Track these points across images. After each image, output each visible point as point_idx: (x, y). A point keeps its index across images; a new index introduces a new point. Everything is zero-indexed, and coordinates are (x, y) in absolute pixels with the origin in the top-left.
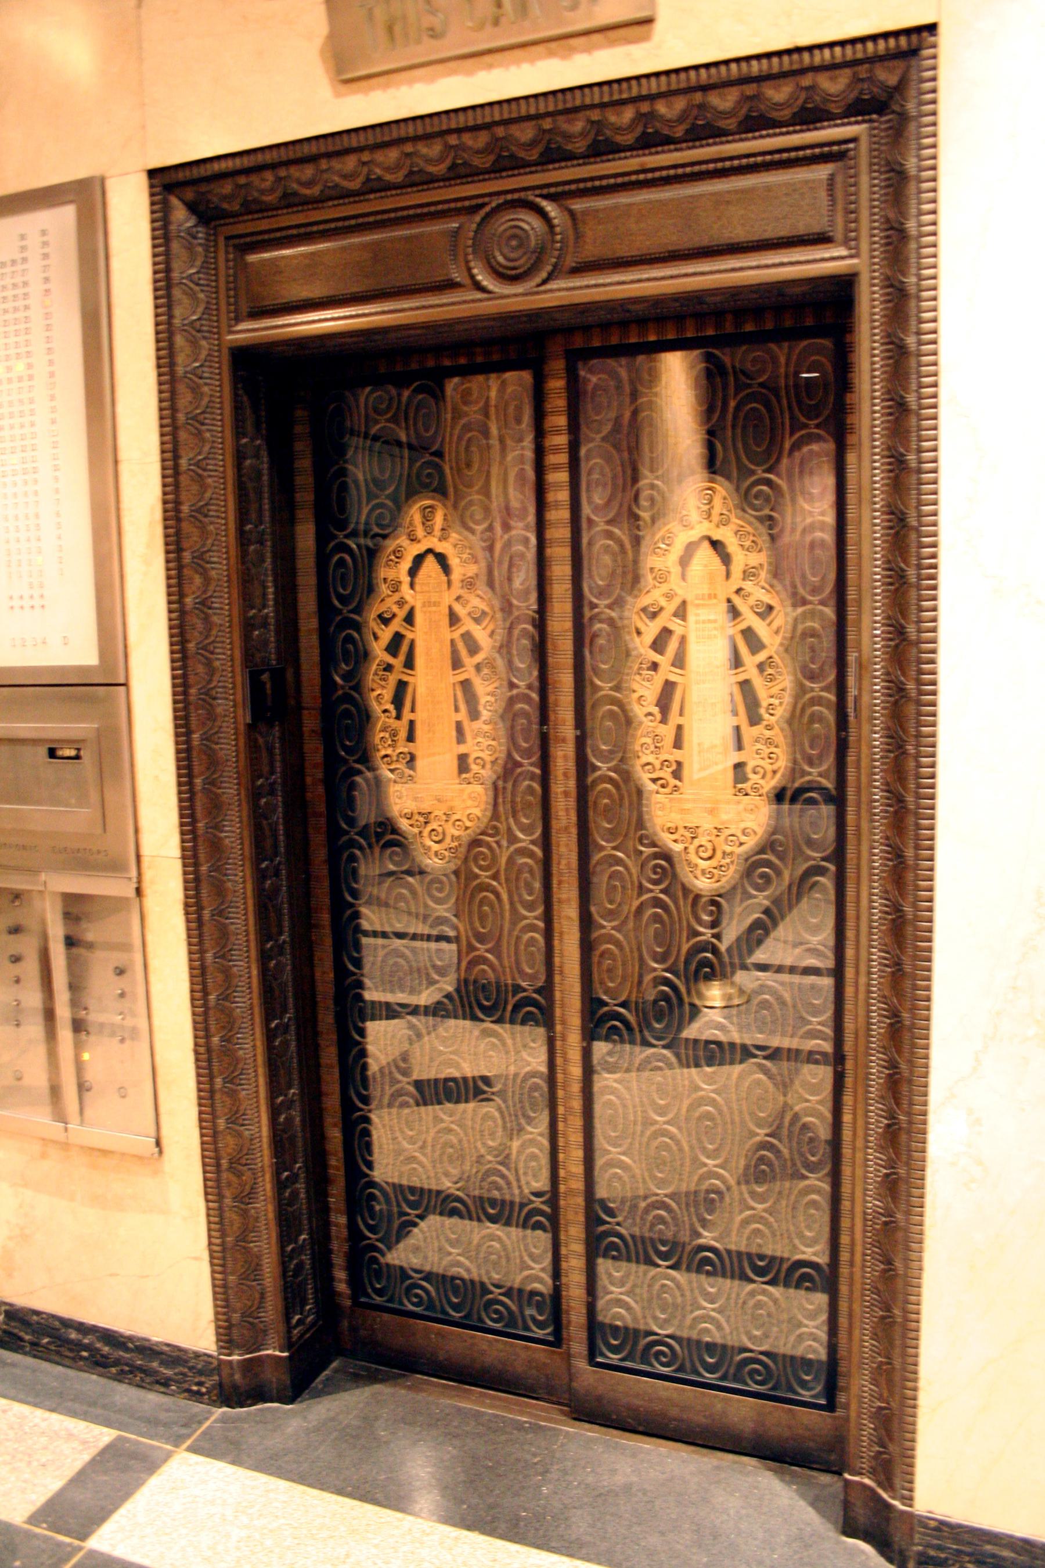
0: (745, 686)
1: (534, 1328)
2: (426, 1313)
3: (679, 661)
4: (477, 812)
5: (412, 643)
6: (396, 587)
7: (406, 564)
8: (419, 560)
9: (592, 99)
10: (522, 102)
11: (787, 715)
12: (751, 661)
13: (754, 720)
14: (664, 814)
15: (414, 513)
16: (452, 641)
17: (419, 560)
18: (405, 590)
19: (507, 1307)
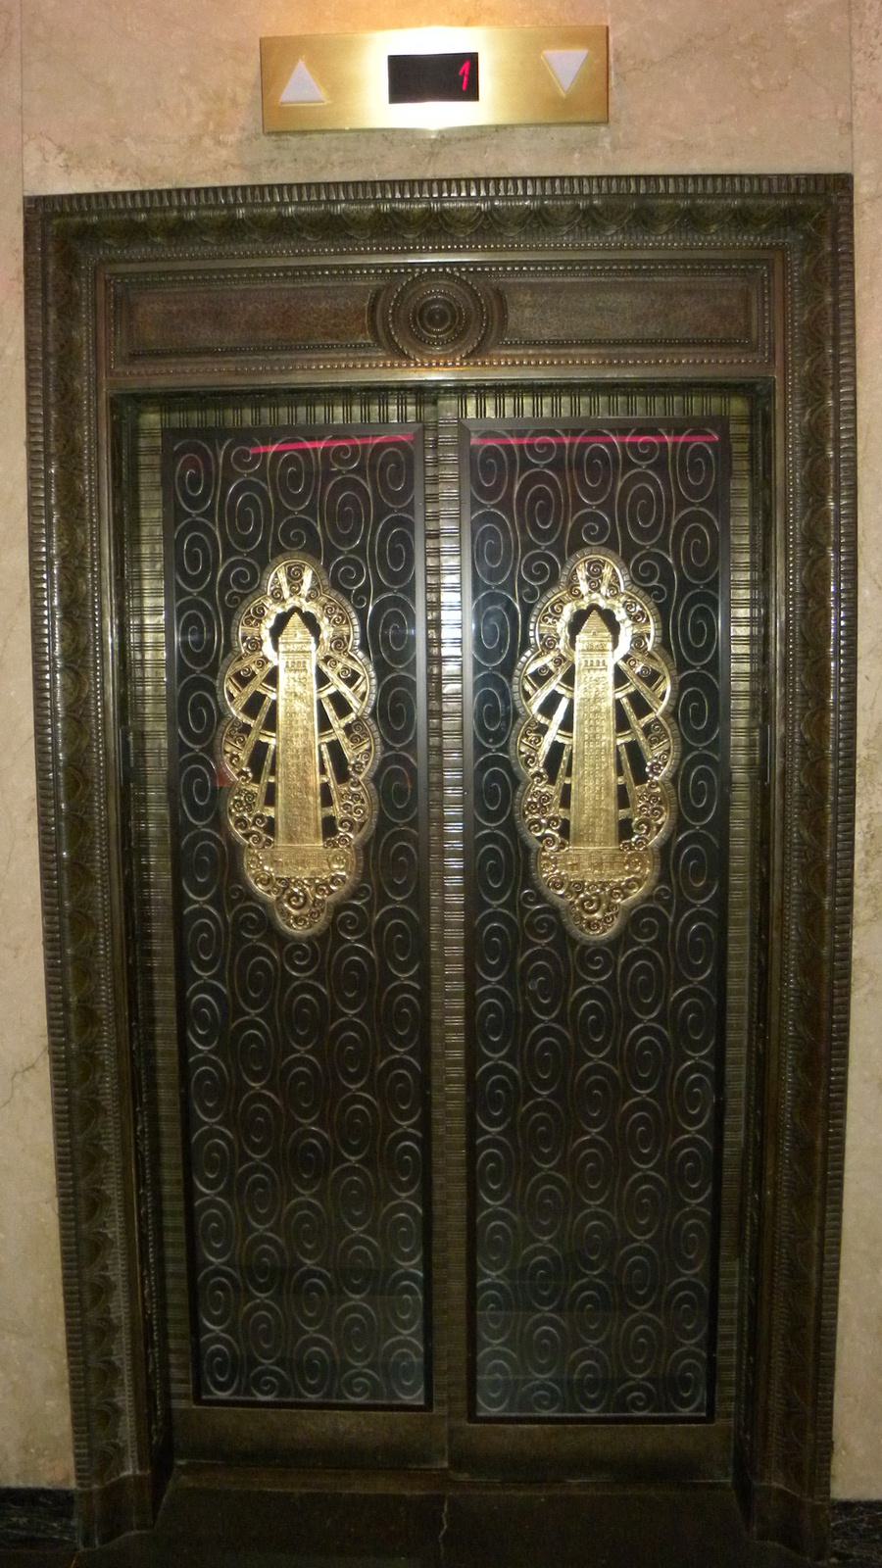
0: (335, 747)
1: (306, 1394)
2: (371, 1402)
3: (271, 724)
4: (339, 870)
5: (275, 704)
6: (257, 644)
7: (269, 623)
8: (282, 621)
9: (752, 189)
10: (719, 180)
11: (671, 775)
12: (338, 724)
13: (640, 777)
14: (261, 869)
15: (279, 575)
16: (618, 703)
17: (282, 621)
18: (267, 648)
19: (370, 1378)
